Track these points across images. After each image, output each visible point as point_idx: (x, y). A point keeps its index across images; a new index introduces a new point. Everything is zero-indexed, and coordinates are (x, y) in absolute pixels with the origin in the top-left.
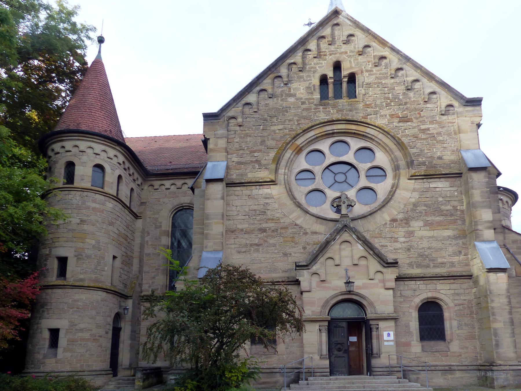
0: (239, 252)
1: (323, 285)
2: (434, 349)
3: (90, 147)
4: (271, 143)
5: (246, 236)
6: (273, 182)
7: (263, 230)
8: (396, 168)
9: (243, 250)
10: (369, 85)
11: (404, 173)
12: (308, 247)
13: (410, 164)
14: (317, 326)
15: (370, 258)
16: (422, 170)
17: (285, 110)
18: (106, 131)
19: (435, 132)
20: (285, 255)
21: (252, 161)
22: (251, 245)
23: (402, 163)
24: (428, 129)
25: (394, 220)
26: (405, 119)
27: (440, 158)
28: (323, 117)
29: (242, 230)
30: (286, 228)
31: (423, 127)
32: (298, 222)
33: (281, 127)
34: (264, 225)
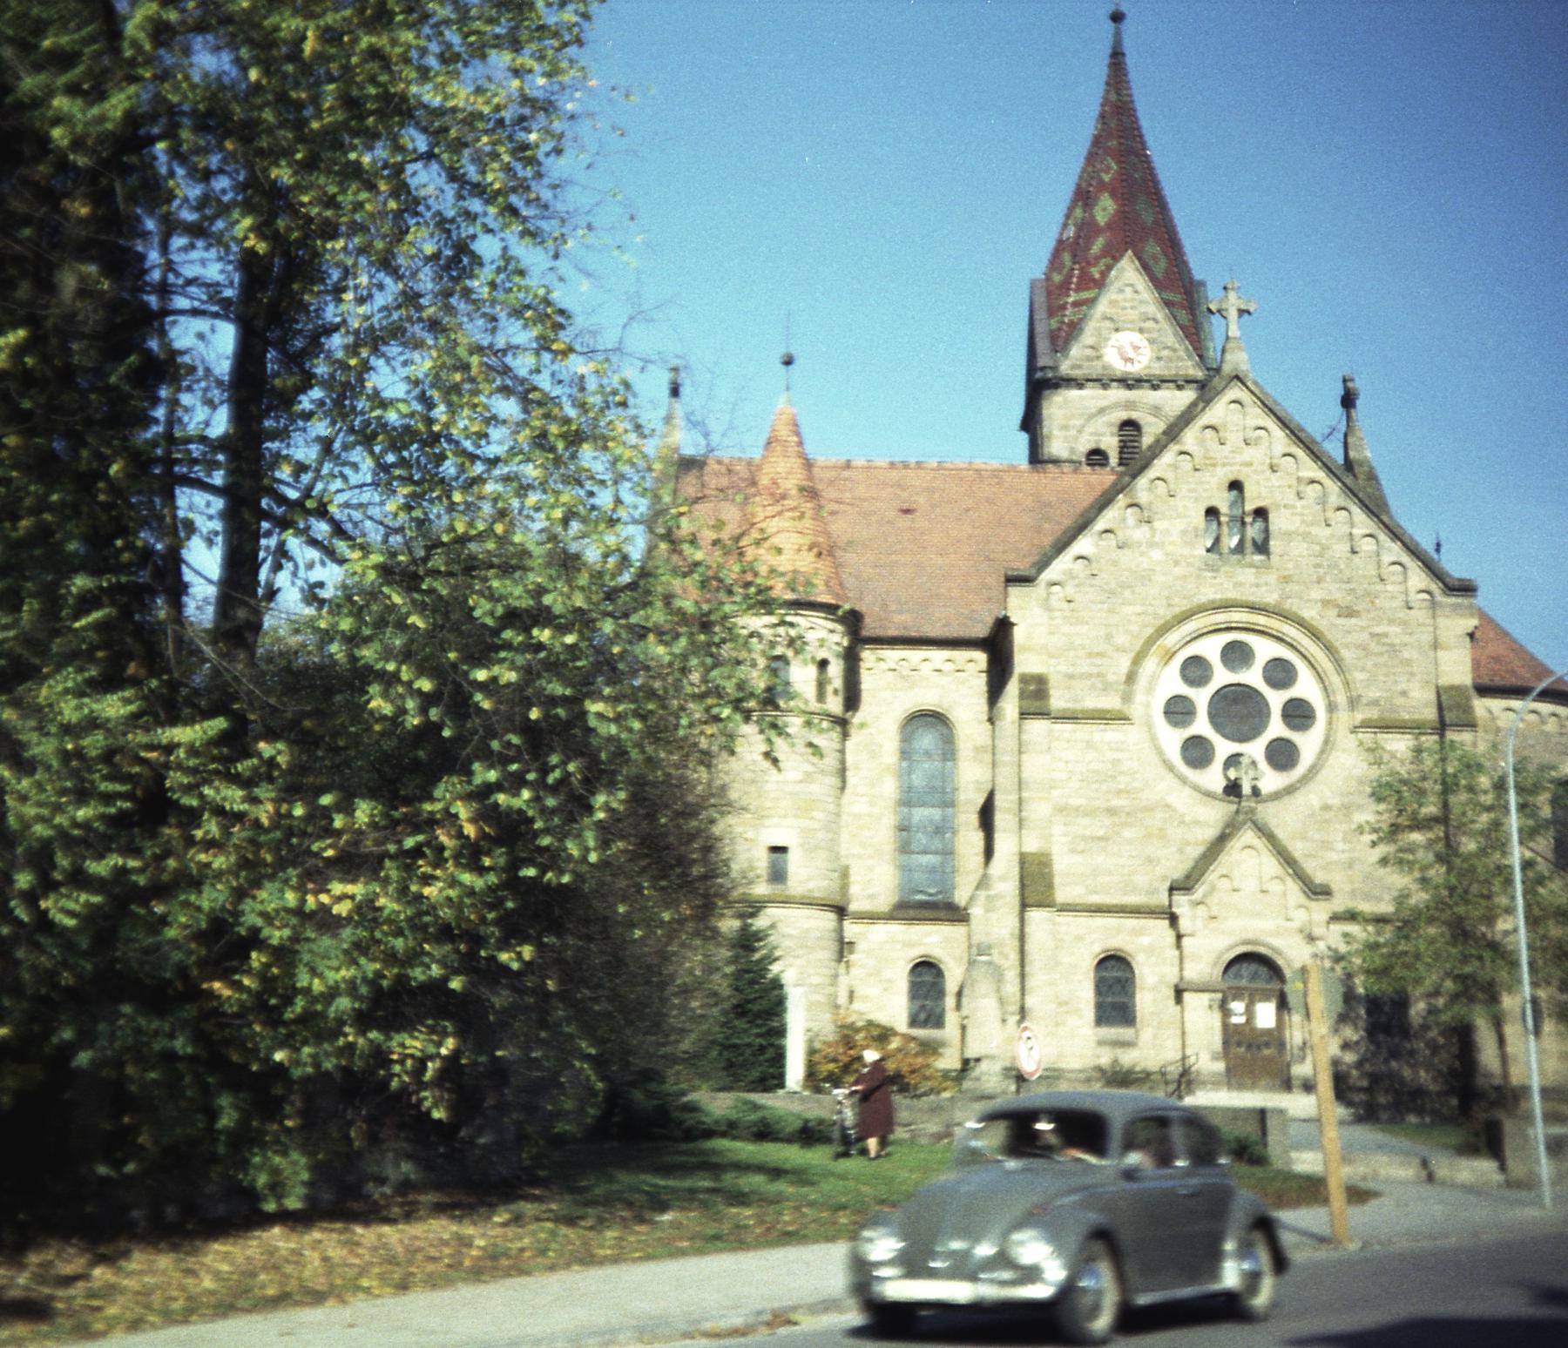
0: (1073, 851)
1: (1214, 924)
2: (600, 1191)
3: (1106, 531)
4: (1121, 639)
5: (1085, 821)
6: (1122, 718)
7: (1111, 811)
8: (1331, 708)
9: (1081, 847)
10: (1288, 535)
11: (1344, 718)
12: (1189, 849)
13: (1353, 703)
14: (1206, 997)
15: (1289, 881)
16: (1373, 714)
17: (1146, 577)
18: (1038, 530)
19: (1397, 641)
20: (1150, 860)
21: (1091, 675)
22: (1093, 838)
23: (1341, 698)
24: (1386, 635)
25: (1326, 808)
26: (1349, 613)
27: (1404, 693)
28: (1209, 594)
29: (1077, 809)
30: (1148, 809)
31: (1378, 630)
32: (1170, 799)
33: (1139, 609)
34: (1116, 802)
